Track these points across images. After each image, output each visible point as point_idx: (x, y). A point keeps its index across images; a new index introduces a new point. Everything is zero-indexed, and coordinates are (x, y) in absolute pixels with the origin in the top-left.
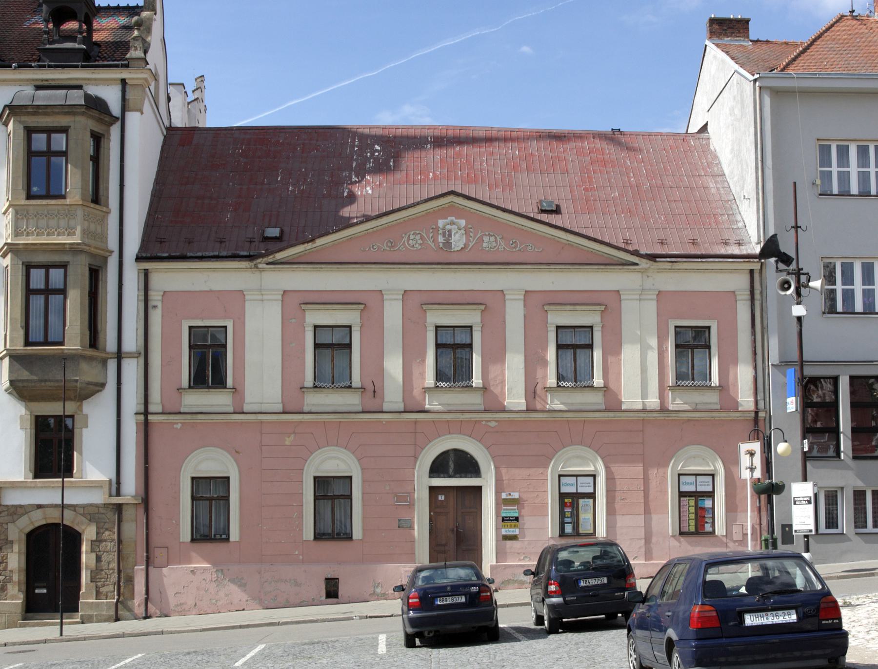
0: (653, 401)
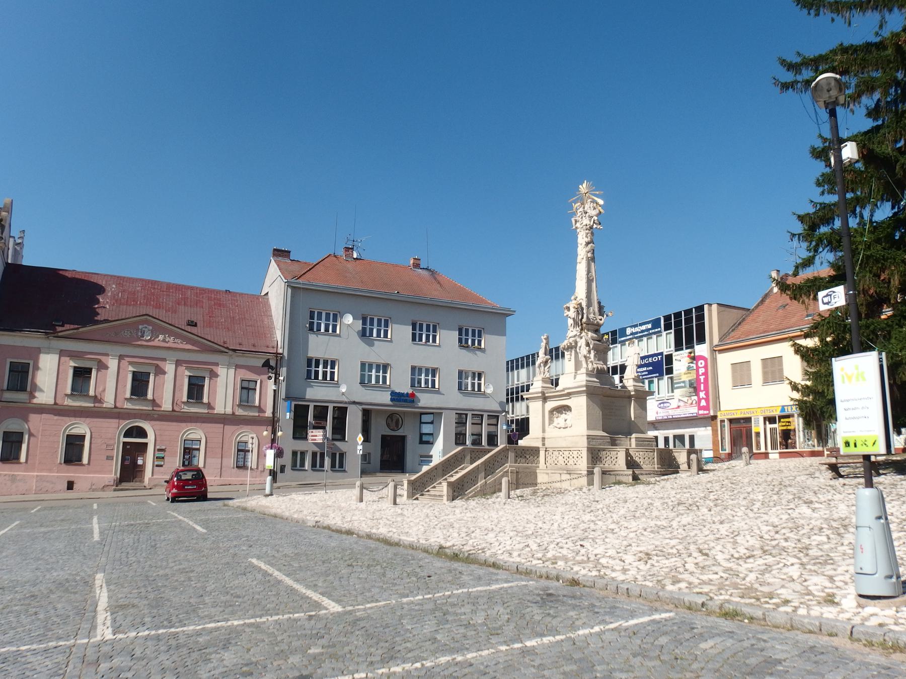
0: (229, 410)
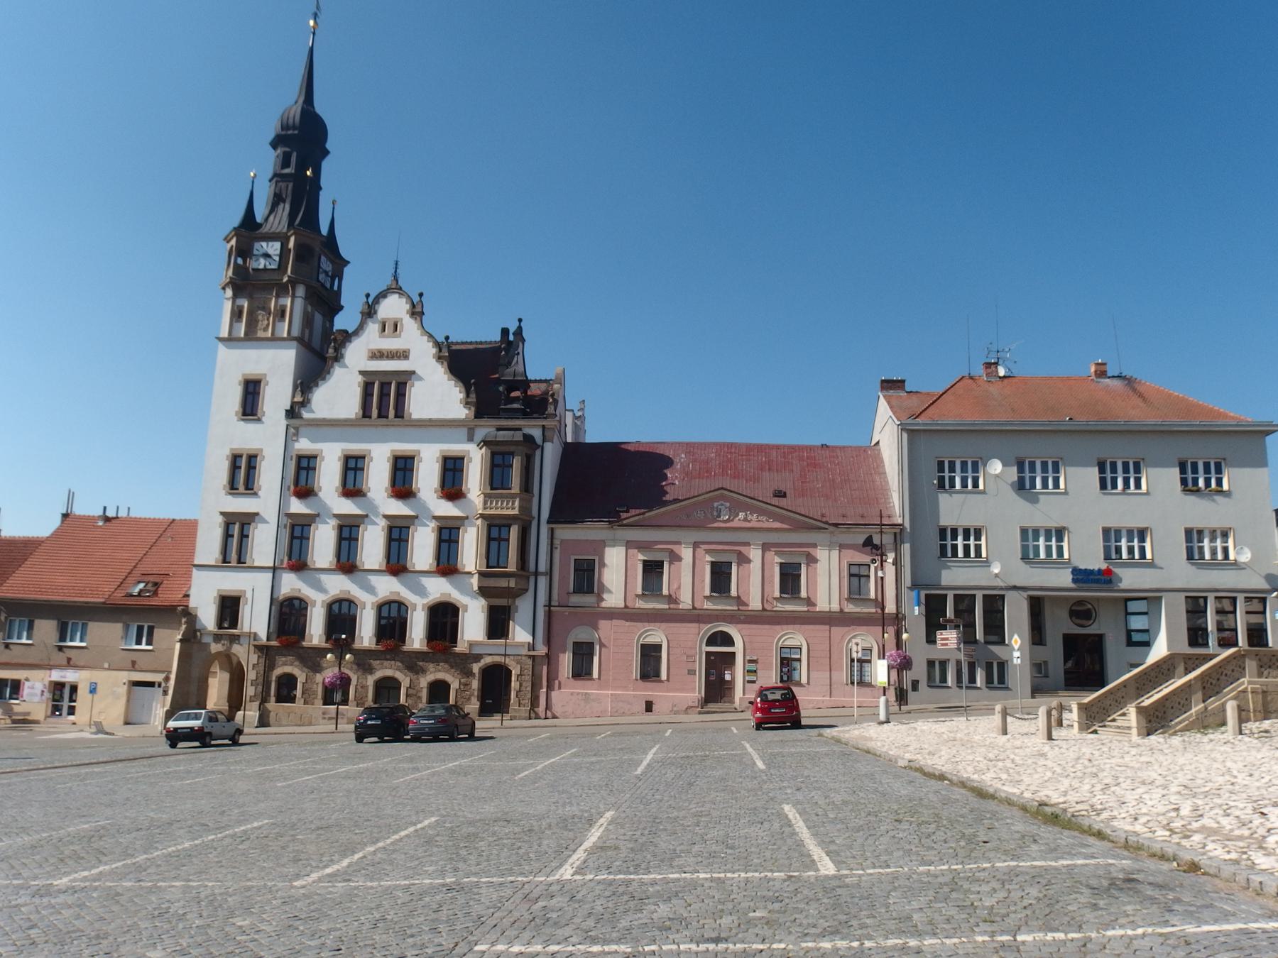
0: (835, 606)
